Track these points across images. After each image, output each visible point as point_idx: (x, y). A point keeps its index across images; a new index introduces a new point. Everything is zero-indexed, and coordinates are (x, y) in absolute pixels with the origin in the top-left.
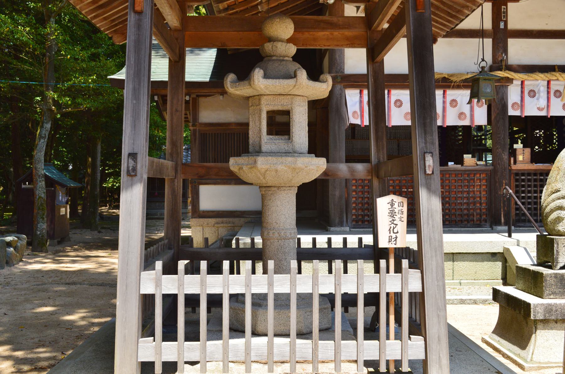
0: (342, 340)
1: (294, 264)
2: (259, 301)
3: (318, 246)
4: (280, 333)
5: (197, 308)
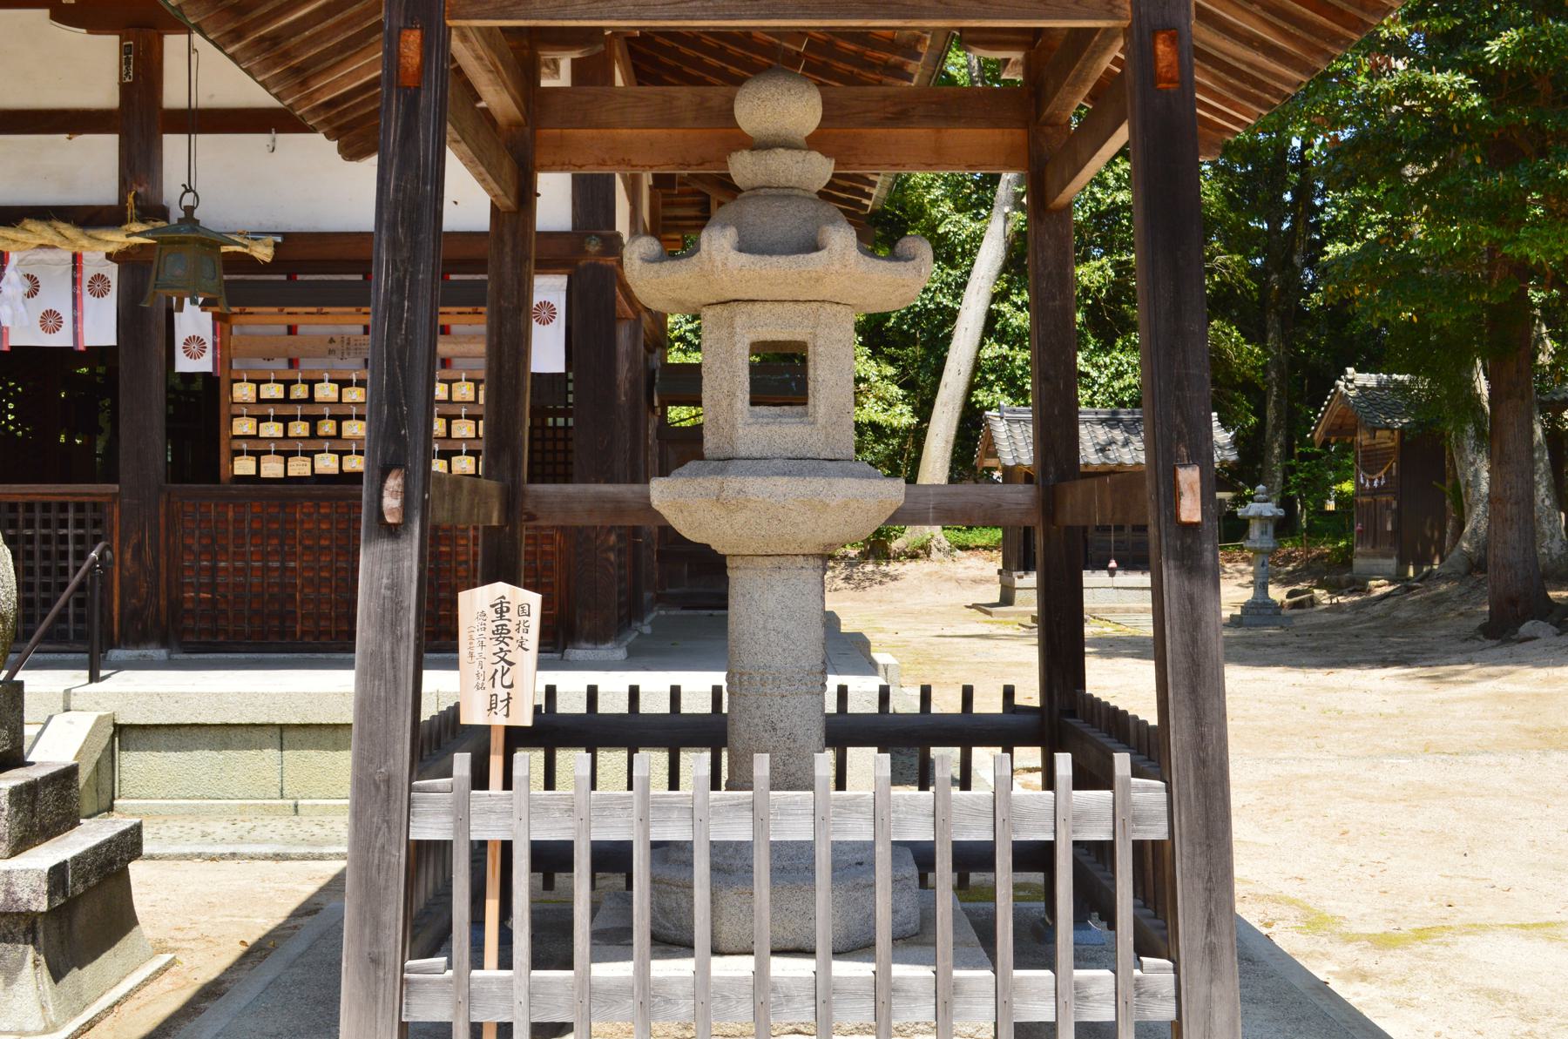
0: (1076, 967)
1: (825, 762)
2: (730, 863)
3: (685, 709)
4: (791, 946)
5: (930, 875)
